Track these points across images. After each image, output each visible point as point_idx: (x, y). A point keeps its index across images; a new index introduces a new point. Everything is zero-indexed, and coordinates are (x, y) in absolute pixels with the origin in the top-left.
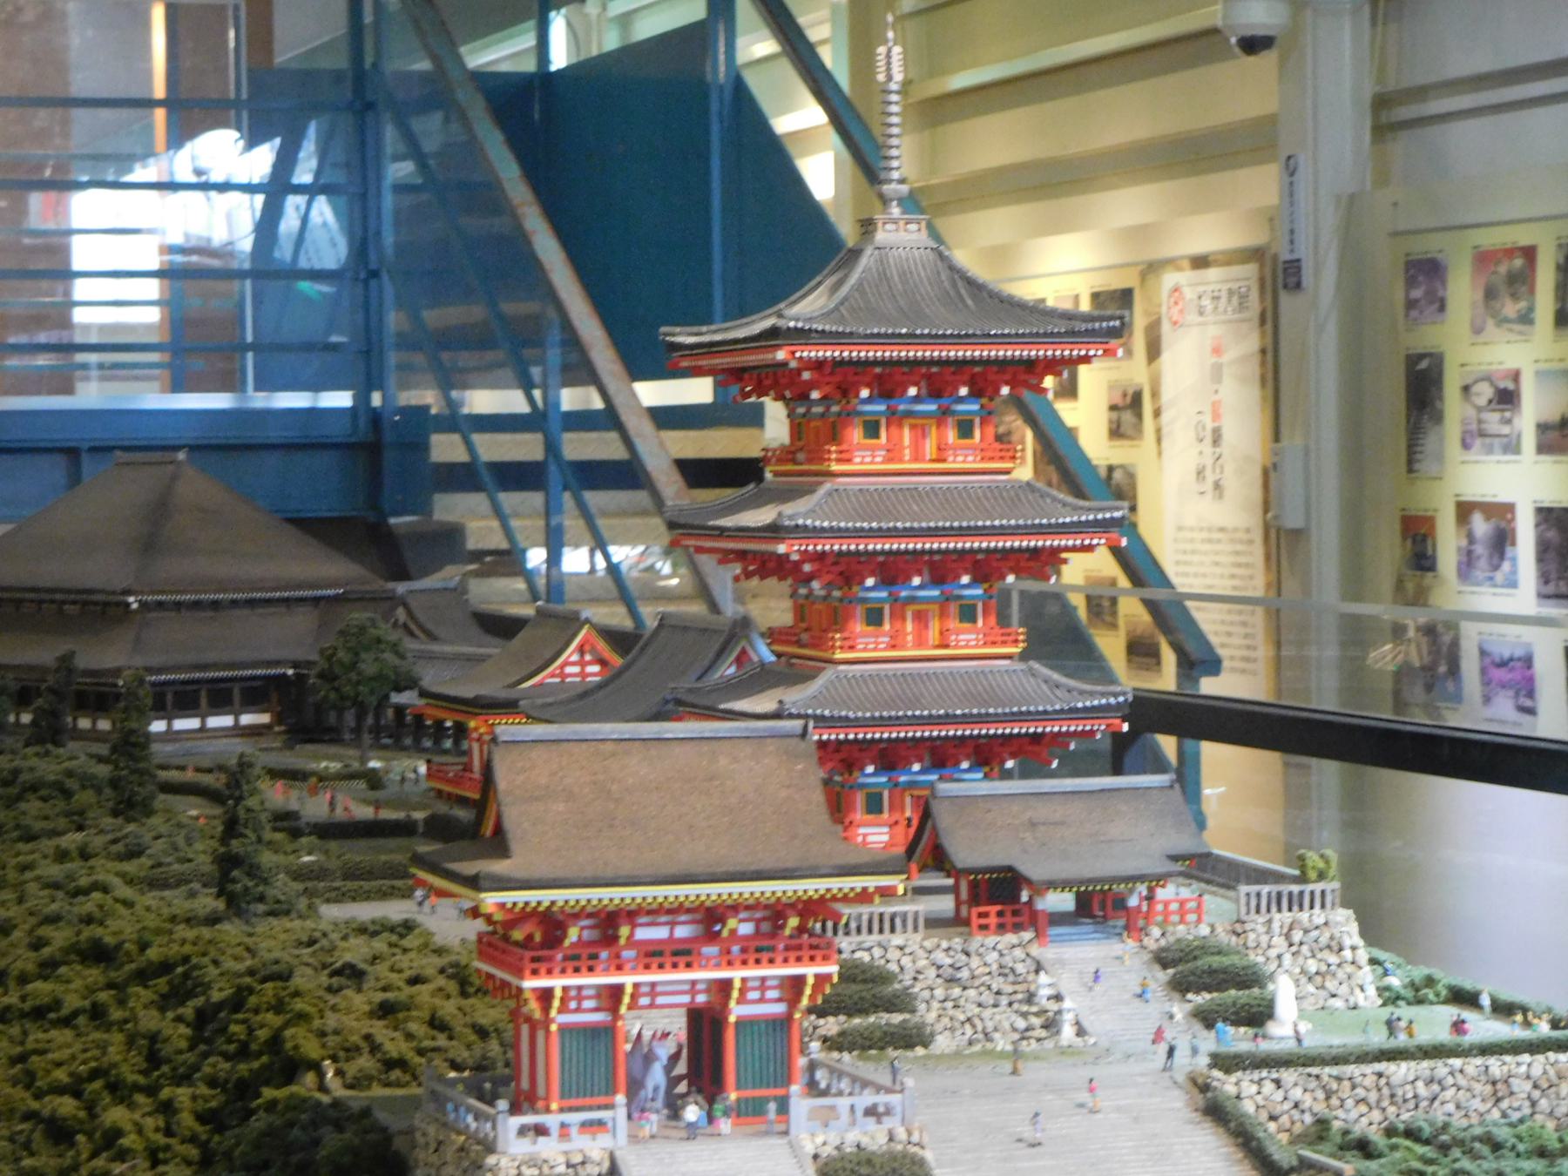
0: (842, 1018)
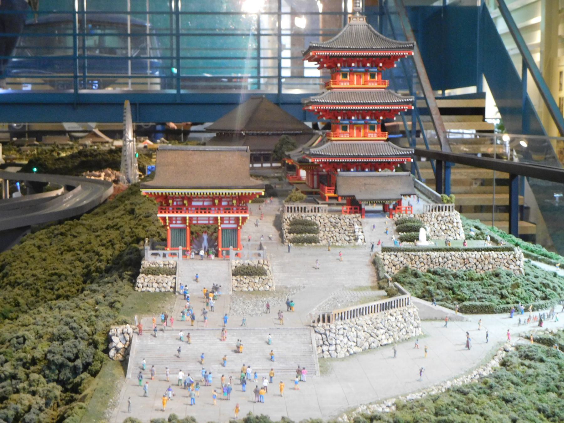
0: (295, 234)
